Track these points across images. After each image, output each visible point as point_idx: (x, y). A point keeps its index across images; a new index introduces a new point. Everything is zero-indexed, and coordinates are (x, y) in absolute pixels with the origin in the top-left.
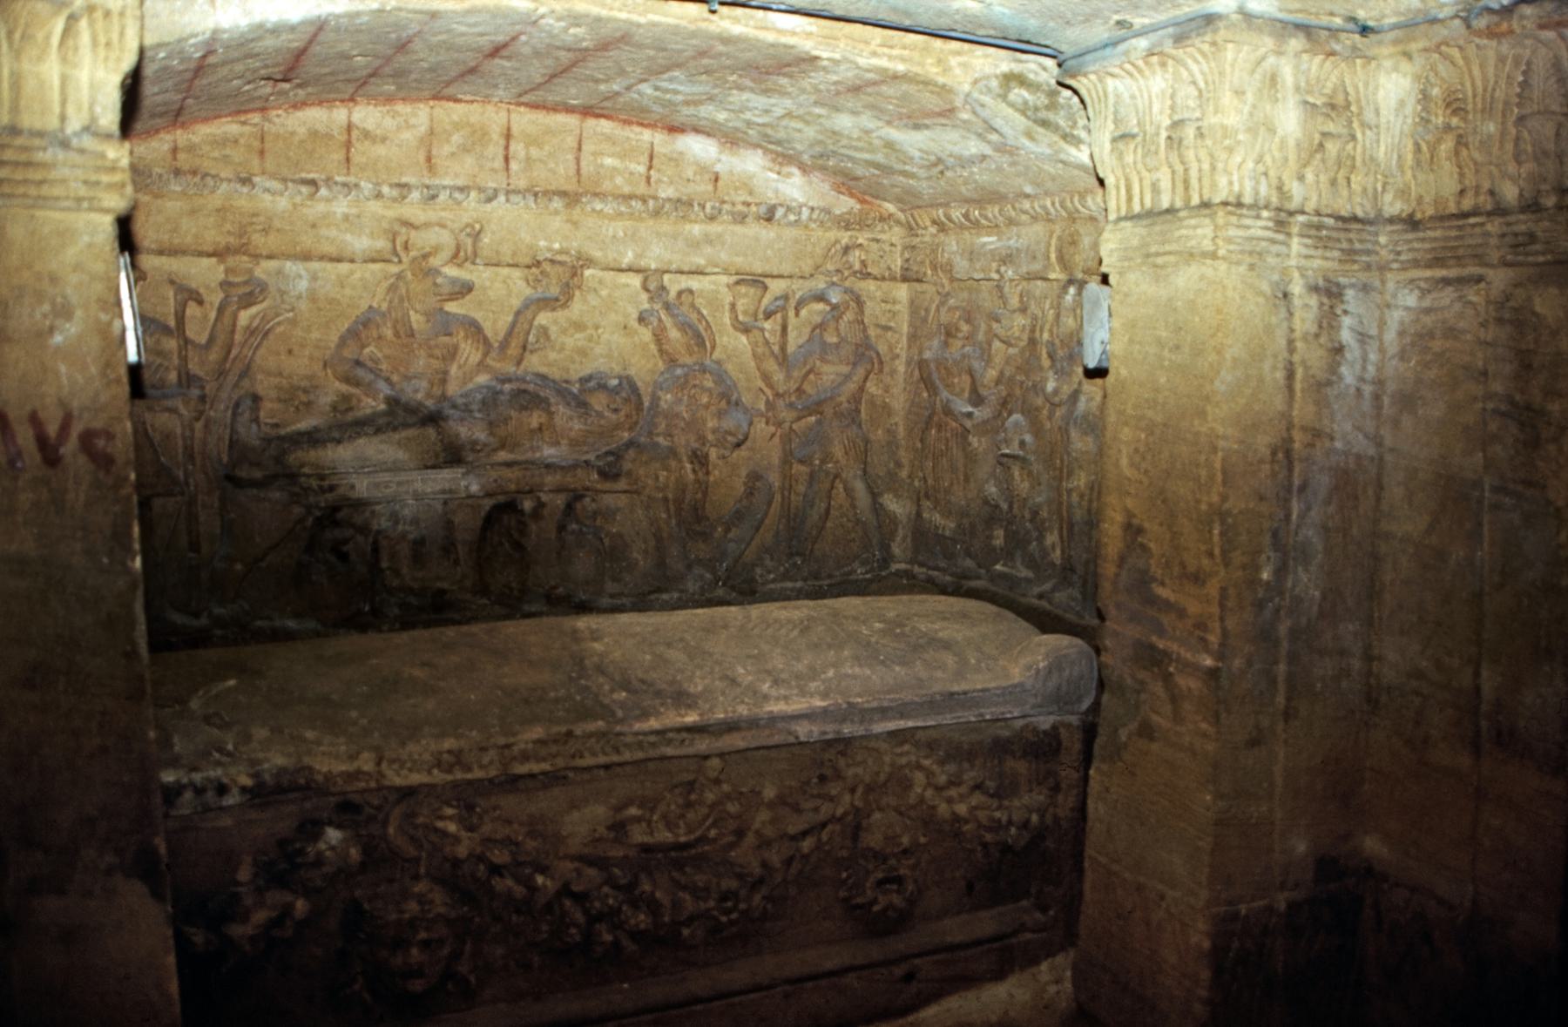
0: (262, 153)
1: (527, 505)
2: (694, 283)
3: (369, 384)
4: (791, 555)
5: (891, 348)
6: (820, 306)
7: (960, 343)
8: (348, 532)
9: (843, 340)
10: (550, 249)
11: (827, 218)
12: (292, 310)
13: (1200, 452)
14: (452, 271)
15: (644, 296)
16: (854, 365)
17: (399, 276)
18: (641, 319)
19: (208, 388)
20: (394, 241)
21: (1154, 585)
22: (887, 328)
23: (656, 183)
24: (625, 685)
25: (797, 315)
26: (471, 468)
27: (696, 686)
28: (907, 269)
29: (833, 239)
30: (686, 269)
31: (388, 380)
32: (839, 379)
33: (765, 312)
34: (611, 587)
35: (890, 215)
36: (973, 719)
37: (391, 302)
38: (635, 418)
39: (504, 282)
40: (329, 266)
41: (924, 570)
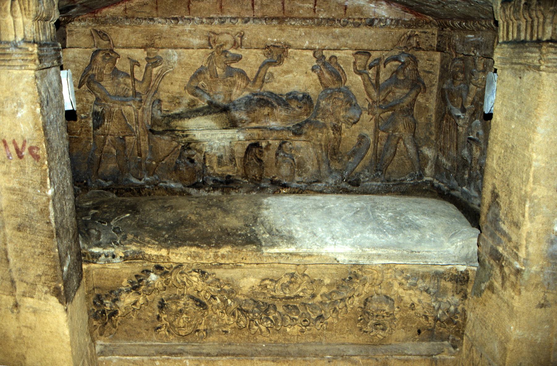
0: (157, 8)
1: (264, 144)
2: (337, 54)
3: (201, 96)
4: (377, 170)
5: (431, 82)
6: (396, 63)
7: (459, 82)
8: (193, 152)
9: (406, 78)
10: (272, 42)
11: (398, 22)
12: (172, 67)
13: (524, 165)
14: (233, 51)
15: (315, 60)
16: (411, 89)
17: (212, 53)
18: (313, 70)
19: (143, 97)
20: (209, 40)
21: (500, 223)
22: (429, 72)
23: (318, 11)
24: (270, 232)
25: (385, 67)
26: (241, 129)
27: (298, 235)
28: (439, 46)
29: (403, 33)
30: (332, 48)
31: (208, 94)
32: (404, 96)
33: (369, 66)
34: (297, 178)
35: (431, 21)
36: (422, 263)
37: (209, 64)
38: (308, 111)
39: (255, 55)
40: (185, 50)
41: (438, 182)
